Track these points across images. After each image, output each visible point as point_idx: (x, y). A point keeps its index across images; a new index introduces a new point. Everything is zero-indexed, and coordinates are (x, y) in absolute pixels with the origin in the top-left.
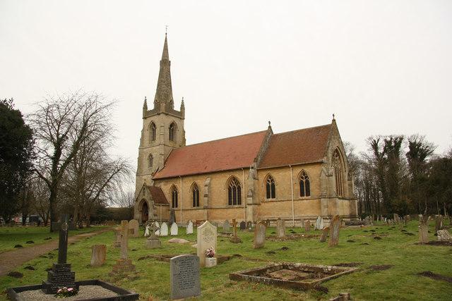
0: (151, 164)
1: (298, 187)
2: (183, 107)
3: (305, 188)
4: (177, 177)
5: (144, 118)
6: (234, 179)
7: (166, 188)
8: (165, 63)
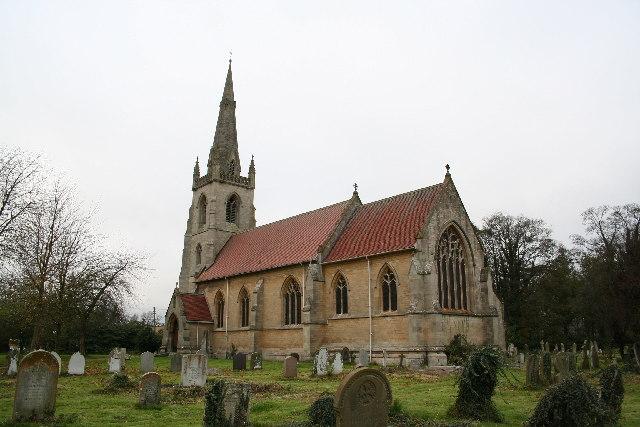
0: (199, 261)
1: (378, 294)
2: (252, 169)
3: (389, 296)
4: (222, 280)
5: (194, 189)
6: (293, 281)
7: (210, 296)
8: (228, 104)
